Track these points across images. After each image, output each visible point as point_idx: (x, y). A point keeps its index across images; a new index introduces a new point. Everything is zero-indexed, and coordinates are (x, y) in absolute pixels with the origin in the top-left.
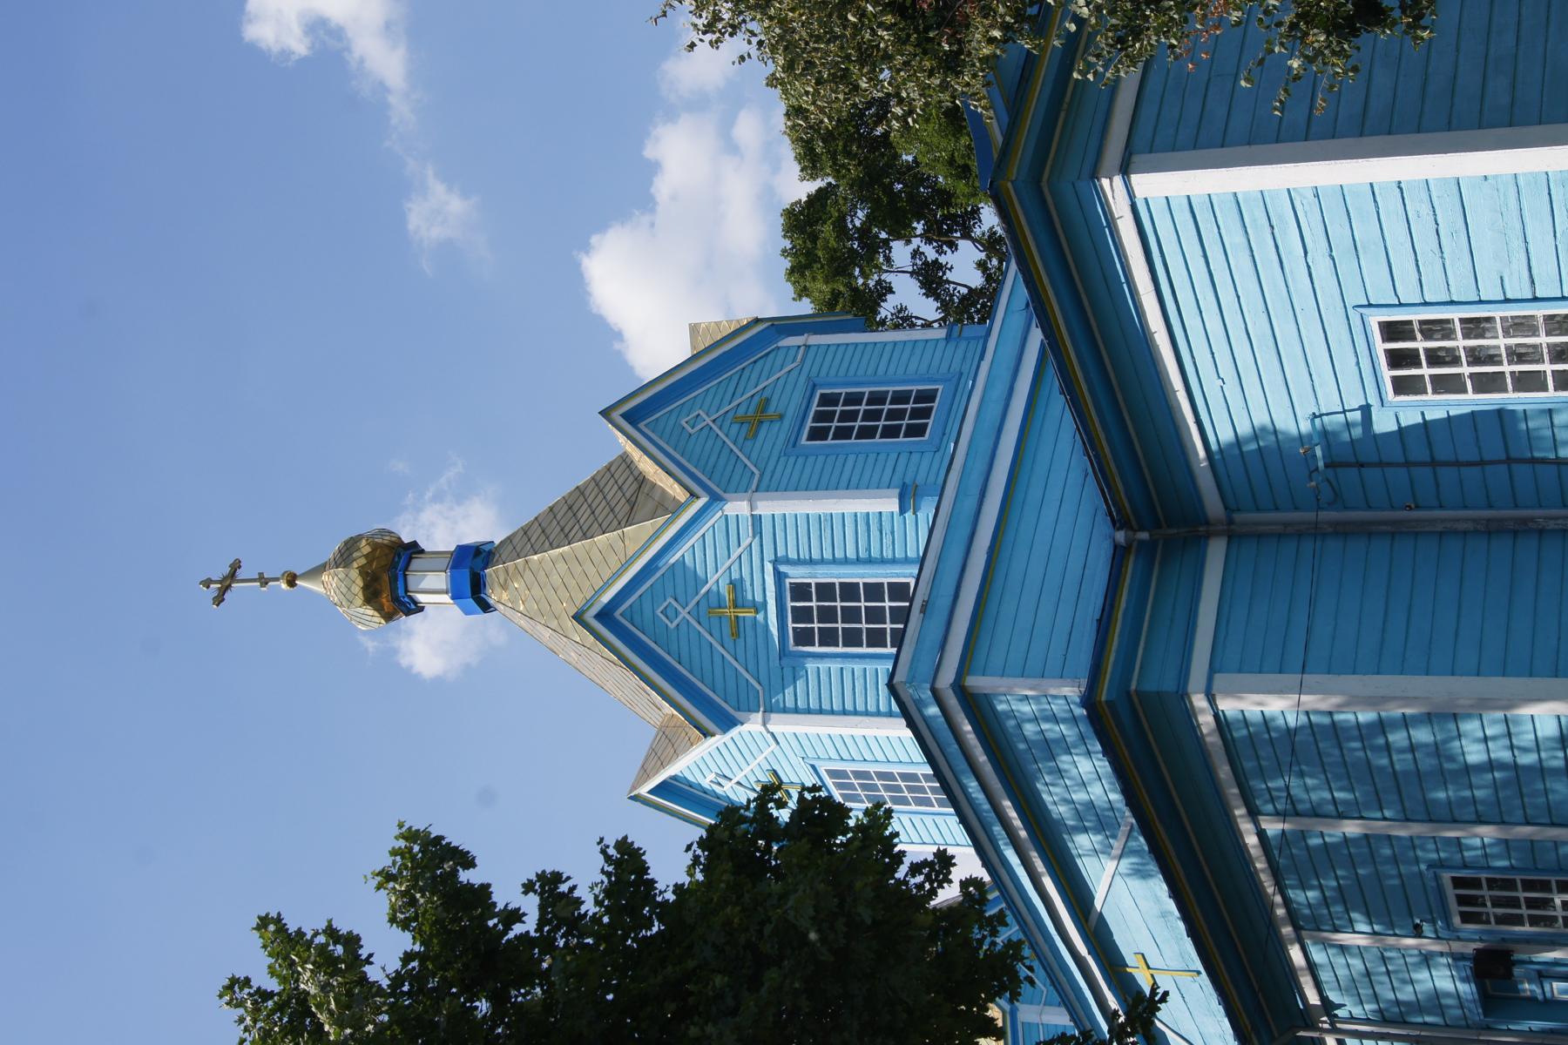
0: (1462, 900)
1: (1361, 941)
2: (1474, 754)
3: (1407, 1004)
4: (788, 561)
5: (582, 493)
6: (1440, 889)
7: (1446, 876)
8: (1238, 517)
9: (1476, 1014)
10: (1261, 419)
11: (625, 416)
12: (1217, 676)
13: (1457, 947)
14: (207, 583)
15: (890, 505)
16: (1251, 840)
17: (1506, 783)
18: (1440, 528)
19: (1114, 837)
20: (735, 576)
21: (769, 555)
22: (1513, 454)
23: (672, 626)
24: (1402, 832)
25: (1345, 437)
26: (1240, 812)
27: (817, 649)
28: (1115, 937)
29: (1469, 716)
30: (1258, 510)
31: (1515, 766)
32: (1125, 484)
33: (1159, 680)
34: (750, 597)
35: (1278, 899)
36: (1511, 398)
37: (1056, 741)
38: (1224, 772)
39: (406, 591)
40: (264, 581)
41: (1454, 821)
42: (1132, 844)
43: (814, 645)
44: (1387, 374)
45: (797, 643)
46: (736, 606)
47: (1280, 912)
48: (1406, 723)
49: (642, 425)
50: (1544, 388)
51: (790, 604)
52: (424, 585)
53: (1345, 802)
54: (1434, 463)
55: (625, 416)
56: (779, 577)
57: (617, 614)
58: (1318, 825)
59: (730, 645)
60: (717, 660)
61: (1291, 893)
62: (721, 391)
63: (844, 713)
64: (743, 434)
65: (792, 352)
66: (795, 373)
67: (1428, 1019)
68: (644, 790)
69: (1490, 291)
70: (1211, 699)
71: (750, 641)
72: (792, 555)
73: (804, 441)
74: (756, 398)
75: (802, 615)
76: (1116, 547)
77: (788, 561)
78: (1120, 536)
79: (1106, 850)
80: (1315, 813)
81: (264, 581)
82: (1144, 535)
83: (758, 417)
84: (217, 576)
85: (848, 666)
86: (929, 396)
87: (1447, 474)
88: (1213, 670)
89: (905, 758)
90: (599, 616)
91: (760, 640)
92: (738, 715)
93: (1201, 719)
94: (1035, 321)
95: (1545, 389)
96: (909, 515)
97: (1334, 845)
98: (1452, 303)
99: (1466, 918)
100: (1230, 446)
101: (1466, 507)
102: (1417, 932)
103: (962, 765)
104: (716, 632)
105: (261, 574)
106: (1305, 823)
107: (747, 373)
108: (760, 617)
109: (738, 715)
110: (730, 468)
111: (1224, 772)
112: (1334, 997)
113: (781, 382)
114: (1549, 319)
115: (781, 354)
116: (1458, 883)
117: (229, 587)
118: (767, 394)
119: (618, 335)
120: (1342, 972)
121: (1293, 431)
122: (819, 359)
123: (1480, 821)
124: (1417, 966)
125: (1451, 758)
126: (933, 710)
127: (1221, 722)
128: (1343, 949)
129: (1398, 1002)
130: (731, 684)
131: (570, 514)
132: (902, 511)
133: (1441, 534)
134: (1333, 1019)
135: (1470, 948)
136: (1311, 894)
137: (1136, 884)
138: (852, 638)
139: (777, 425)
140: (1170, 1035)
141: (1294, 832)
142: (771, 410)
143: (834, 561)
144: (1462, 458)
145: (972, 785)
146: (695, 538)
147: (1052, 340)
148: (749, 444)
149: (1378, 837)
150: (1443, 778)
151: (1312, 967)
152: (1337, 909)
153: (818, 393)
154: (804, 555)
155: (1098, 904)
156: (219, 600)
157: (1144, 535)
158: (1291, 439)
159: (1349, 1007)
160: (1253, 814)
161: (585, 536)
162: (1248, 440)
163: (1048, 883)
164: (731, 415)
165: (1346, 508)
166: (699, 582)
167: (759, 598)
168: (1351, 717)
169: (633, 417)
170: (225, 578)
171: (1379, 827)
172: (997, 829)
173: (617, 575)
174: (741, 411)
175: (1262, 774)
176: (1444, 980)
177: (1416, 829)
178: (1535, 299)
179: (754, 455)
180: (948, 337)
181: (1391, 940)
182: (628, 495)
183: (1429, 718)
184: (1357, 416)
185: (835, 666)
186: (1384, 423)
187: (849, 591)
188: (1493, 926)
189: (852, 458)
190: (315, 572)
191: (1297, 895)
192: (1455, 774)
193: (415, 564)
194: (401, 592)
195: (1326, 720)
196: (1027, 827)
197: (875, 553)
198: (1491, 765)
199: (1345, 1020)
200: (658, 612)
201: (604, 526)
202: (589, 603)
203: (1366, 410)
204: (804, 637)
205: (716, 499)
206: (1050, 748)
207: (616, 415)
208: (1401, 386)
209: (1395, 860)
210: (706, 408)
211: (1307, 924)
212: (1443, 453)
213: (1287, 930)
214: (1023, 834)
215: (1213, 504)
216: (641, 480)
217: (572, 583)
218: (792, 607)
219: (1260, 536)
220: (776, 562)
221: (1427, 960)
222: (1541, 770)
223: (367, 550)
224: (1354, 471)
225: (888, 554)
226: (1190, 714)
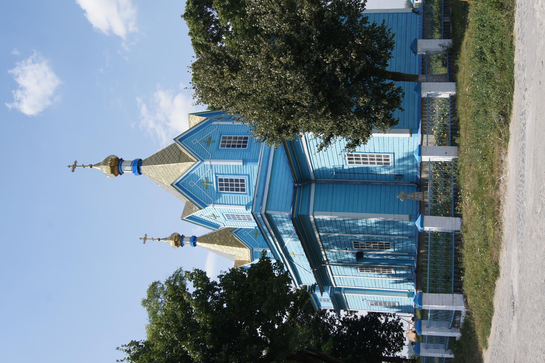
1: (335, 251)
2: (360, 224)
3: (343, 260)
4: (218, 174)
5: (165, 151)
6: (351, 243)
7: (353, 242)
8: (317, 180)
9: (356, 261)
10: (324, 166)
11: (179, 140)
12: (315, 212)
13: (353, 252)
14: (69, 166)
15: (241, 164)
16: (317, 236)
17: (365, 229)
18: (354, 183)
19: (291, 235)
20: (206, 176)
21: (214, 172)
22: (368, 173)
23: (192, 186)
24: (346, 235)
25: (339, 169)
26: (316, 232)
27: (224, 192)
28: (288, 250)
29: (360, 219)
30: (321, 178)
31: (367, 226)
32: (296, 171)
33: (304, 212)
34: (210, 181)
35: (321, 244)
36: (369, 165)
37: (282, 221)
38: (314, 226)
39: (121, 170)
40: (84, 166)
41: (355, 234)
42: (294, 236)
43: (224, 191)
44: (347, 161)
45: (220, 190)
46: (207, 183)
47: (321, 246)
48: (348, 220)
49: (182, 142)
50: (375, 164)
51: (218, 183)
52: (125, 169)
53: (336, 231)
55: (179, 140)
56: (216, 177)
57: (180, 184)
58: (330, 234)
59: (205, 190)
60: (203, 193)
61: (323, 244)
62: (200, 134)
63: (230, 204)
64: (206, 145)
65: (215, 126)
66: (216, 131)
67: (346, 262)
68: (184, 218)
70: (313, 216)
71: (210, 190)
72: (219, 173)
73: (220, 148)
74: (208, 137)
75: (221, 185)
77: (218, 174)
79: (289, 237)
80: (330, 232)
81: (84, 166)
82: (300, 185)
83: (209, 141)
84: (72, 165)
85: (231, 195)
86: (246, 138)
87: (356, 175)
88: (314, 211)
89: (242, 212)
91: (212, 191)
92: (207, 205)
93: (311, 219)
95: (375, 164)
96: (245, 166)
97: (333, 237)
98: (360, 152)
99: (355, 247)
100: (317, 169)
101: (359, 180)
102: (346, 249)
103: (264, 224)
104: (202, 188)
106: (328, 234)
107: (205, 130)
108: (212, 185)
109: (207, 205)
110: (204, 154)
111: (314, 226)
112: (329, 259)
113: (213, 133)
115: (213, 126)
116: (354, 242)
117: (75, 167)
118: (210, 136)
119: (84, 11)
120: (331, 255)
121: (330, 168)
122: (221, 128)
123: (360, 234)
124: (345, 254)
125: (356, 225)
126: (260, 216)
127: (315, 220)
128: (332, 252)
129: (341, 260)
130: (206, 198)
131: (162, 156)
132: (243, 165)
133: (354, 184)
134: (328, 262)
135: (356, 252)
136: (327, 244)
137: (294, 242)
138: (232, 190)
139: (213, 144)
140: (296, 265)
141: (325, 235)
142: (212, 139)
143: (228, 174)
144: (359, 173)
145: (265, 227)
146: (197, 169)
148: (208, 148)
149: (341, 236)
150: (354, 228)
151: (326, 255)
152: (332, 246)
153: (222, 136)
154: (222, 173)
155: (286, 245)
156: (73, 171)
157: (300, 185)
158: (328, 169)
159: (331, 260)
160: (318, 232)
161: (168, 163)
162: (321, 169)
163: (277, 243)
164: (203, 140)
165: (337, 179)
166: (198, 178)
167: (212, 181)
168: (339, 219)
170: (74, 165)
171: (342, 234)
172: (268, 234)
173: (181, 176)
174: (205, 140)
175: (321, 226)
176: (350, 256)
177: (348, 235)
178: (375, 153)
179: (209, 150)
181: (341, 251)
182: (178, 154)
183: (353, 220)
184: (341, 166)
185: (228, 195)
186: (346, 167)
187: (232, 180)
188: (360, 248)
189: (231, 152)
190: (98, 165)
191: (325, 244)
192: (356, 227)
193: (123, 164)
194: (120, 171)
195: (334, 219)
196: (275, 234)
197: (237, 173)
198: (363, 226)
199: (331, 262)
200: (189, 183)
201: (173, 161)
202: (174, 182)
203: (343, 166)
204: (222, 189)
205: (202, 161)
206: (281, 222)
207: (177, 140)
208: (349, 163)
209: (344, 239)
210: (197, 138)
211: (325, 248)
212: (356, 172)
213: (322, 249)
214: (274, 235)
215: (313, 177)
216: (181, 152)
217: (165, 173)
218: (219, 183)
219: (321, 183)
220: (215, 174)
221: (347, 253)
222: (371, 227)
224: (340, 174)
225: (240, 173)
226: (309, 219)
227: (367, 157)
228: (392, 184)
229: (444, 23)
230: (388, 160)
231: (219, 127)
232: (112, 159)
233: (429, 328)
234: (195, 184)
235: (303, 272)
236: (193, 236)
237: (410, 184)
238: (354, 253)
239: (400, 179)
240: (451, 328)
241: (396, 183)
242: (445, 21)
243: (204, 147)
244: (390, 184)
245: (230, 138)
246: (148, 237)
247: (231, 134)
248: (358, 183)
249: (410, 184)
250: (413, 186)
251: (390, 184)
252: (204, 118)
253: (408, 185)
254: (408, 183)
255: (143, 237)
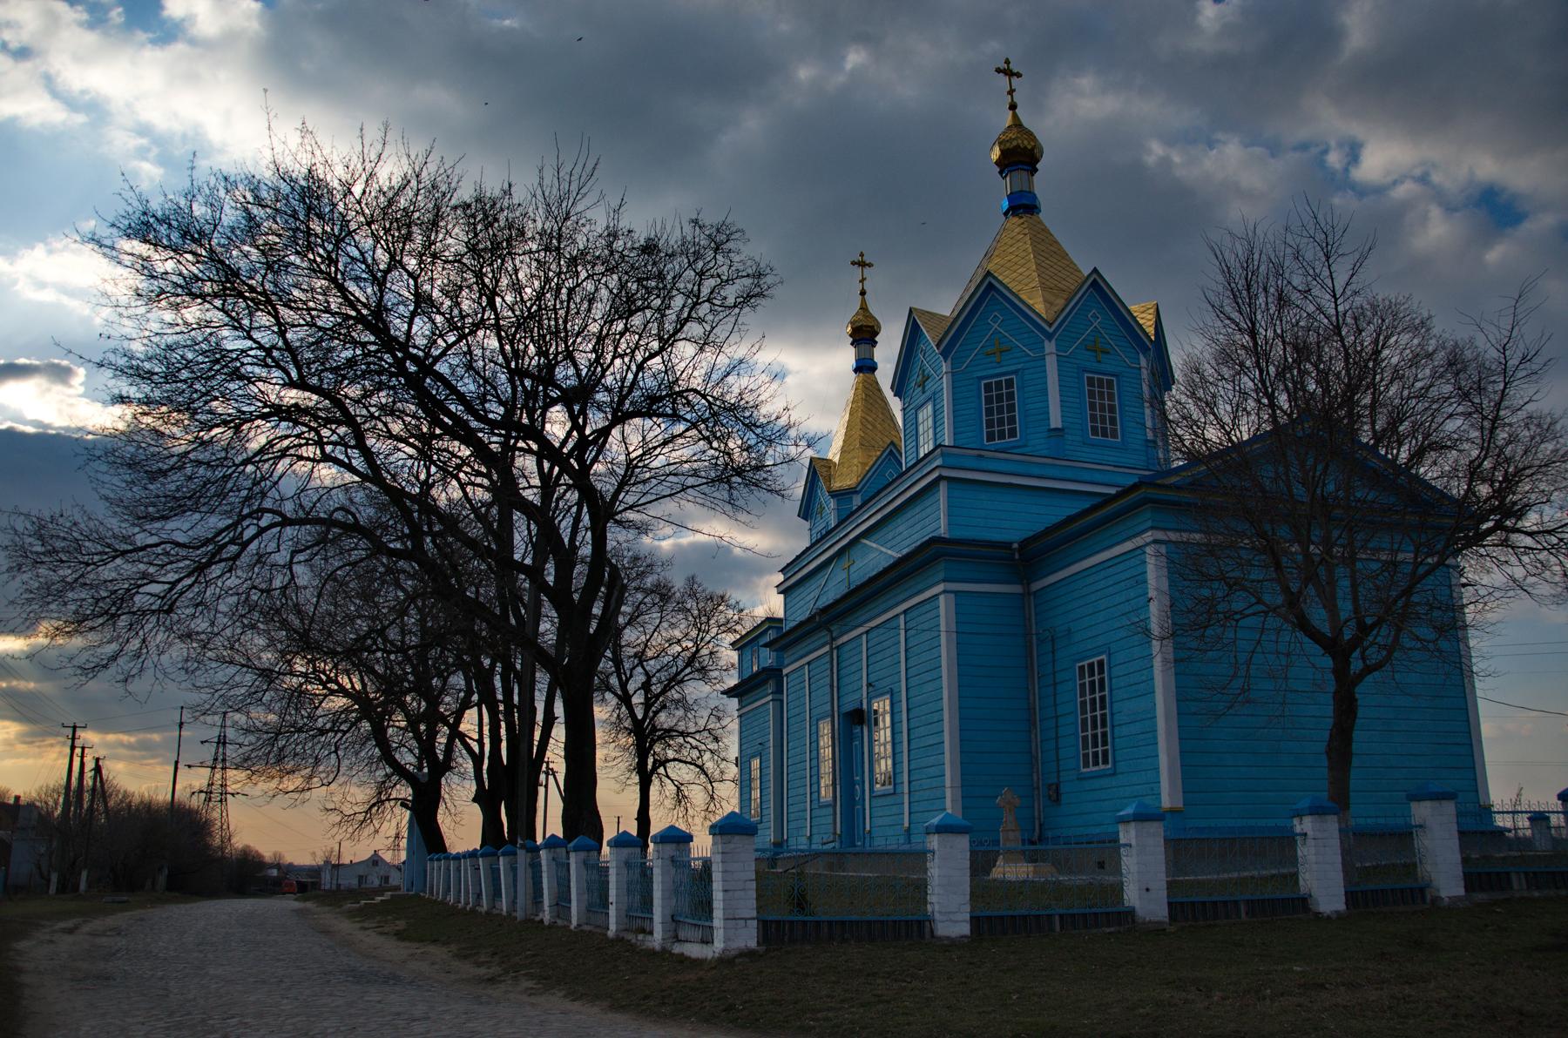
0: (1091, 666)
7: (1104, 657)
11: (1095, 280)
12: (953, 595)
14: (1007, 62)
39: (1011, 171)
54: (1055, 684)
56: (1015, 372)
69: (1116, 706)
76: (1011, 543)
78: (1015, 546)
82: (1017, 556)
88: (956, 593)
90: (990, 283)
94: (1120, 489)
99: (1082, 668)
105: (1014, 90)
114: (1106, 732)
116: (1101, 663)
147: (1108, 500)
156: (998, 71)
157: (1017, 556)
165: (1038, 646)
169: (1095, 284)
170: (1011, 71)
180: (1147, 441)
187: (1011, 408)
189: (1078, 400)
193: (1024, 174)
215: (1036, 586)
223: (1029, 147)
227: (1101, 710)
228: (1035, 778)
229: (1508, 874)
230: (1096, 763)
231: (1135, 371)
232: (1033, 149)
233: (669, 862)
234: (996, 326)
235: (812, 595)
236: (876, 364)
237: (1037, 822)
238: (862, 704)
239: (1050, 797)
240: (673, 920)
241: (1038, 788)
242: (1514, 877)
243: (1084, 340)
244: (1035, 775)
245: (1111, 396)
246: (867, 270)
247: (1119, 397)
248: (1031, 698)
249: (1037, 822)
250: (1034, 830)
251: (1035, 775)
252: (1151, 331)
253: (1034, 818)
254: (1039, 819)
255: (867, 259)
